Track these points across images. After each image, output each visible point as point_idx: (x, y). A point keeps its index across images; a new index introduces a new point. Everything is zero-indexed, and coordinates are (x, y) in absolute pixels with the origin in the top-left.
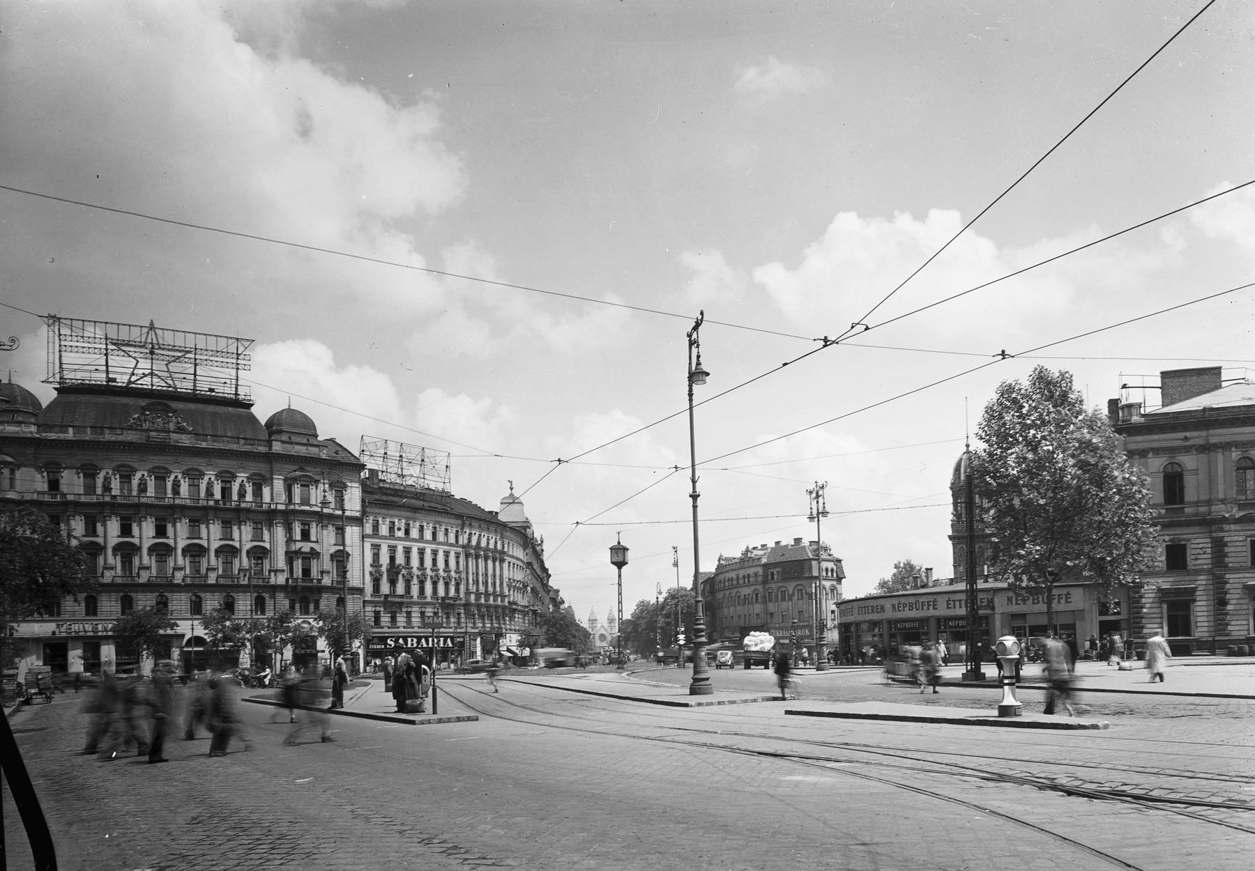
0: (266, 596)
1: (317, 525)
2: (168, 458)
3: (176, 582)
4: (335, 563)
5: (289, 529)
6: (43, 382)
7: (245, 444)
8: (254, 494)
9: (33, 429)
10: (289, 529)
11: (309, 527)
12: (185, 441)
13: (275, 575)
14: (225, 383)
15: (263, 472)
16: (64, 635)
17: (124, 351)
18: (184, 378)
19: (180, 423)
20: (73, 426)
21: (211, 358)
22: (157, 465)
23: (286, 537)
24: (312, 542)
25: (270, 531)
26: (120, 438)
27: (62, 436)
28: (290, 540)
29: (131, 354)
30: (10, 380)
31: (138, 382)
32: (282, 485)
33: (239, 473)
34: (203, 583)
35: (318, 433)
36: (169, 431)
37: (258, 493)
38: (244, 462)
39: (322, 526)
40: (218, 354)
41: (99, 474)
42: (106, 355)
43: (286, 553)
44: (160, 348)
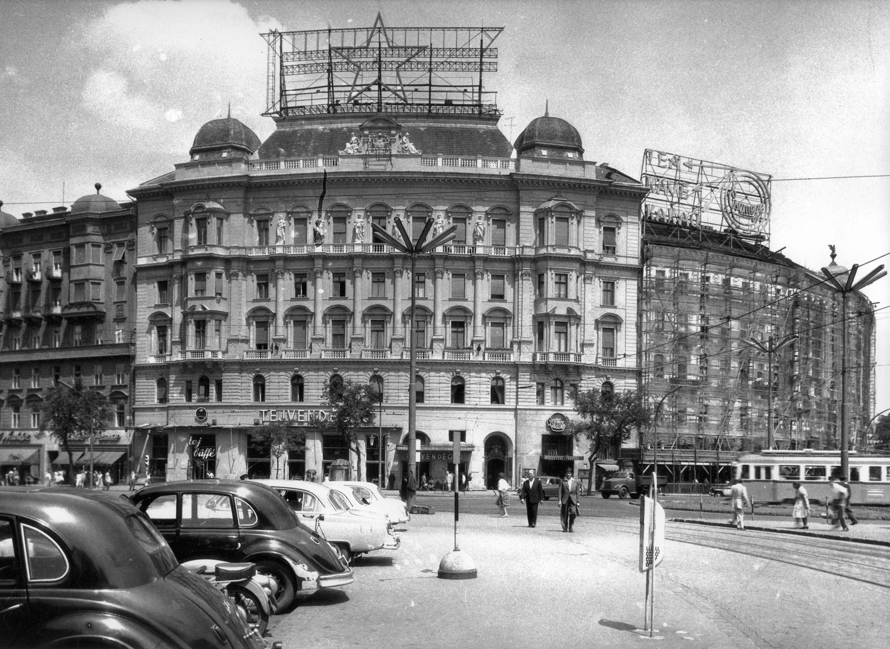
0: (506, 376)
1: (578, 277)
4: (601, 333)
5: (540, 283)
6: (262, 115)
10: (540, 283)
11: (567, 280)
13: (519, 348)
14: (465, 91)
18: (416, 90)
19: (404, 143)
23: (535, 294)
24: (571, 300)
25: (514, 287)
28: (540, 298)
32: (532, 220)
35: (584, 147)
39: (584, 279)
43: (534, 317)
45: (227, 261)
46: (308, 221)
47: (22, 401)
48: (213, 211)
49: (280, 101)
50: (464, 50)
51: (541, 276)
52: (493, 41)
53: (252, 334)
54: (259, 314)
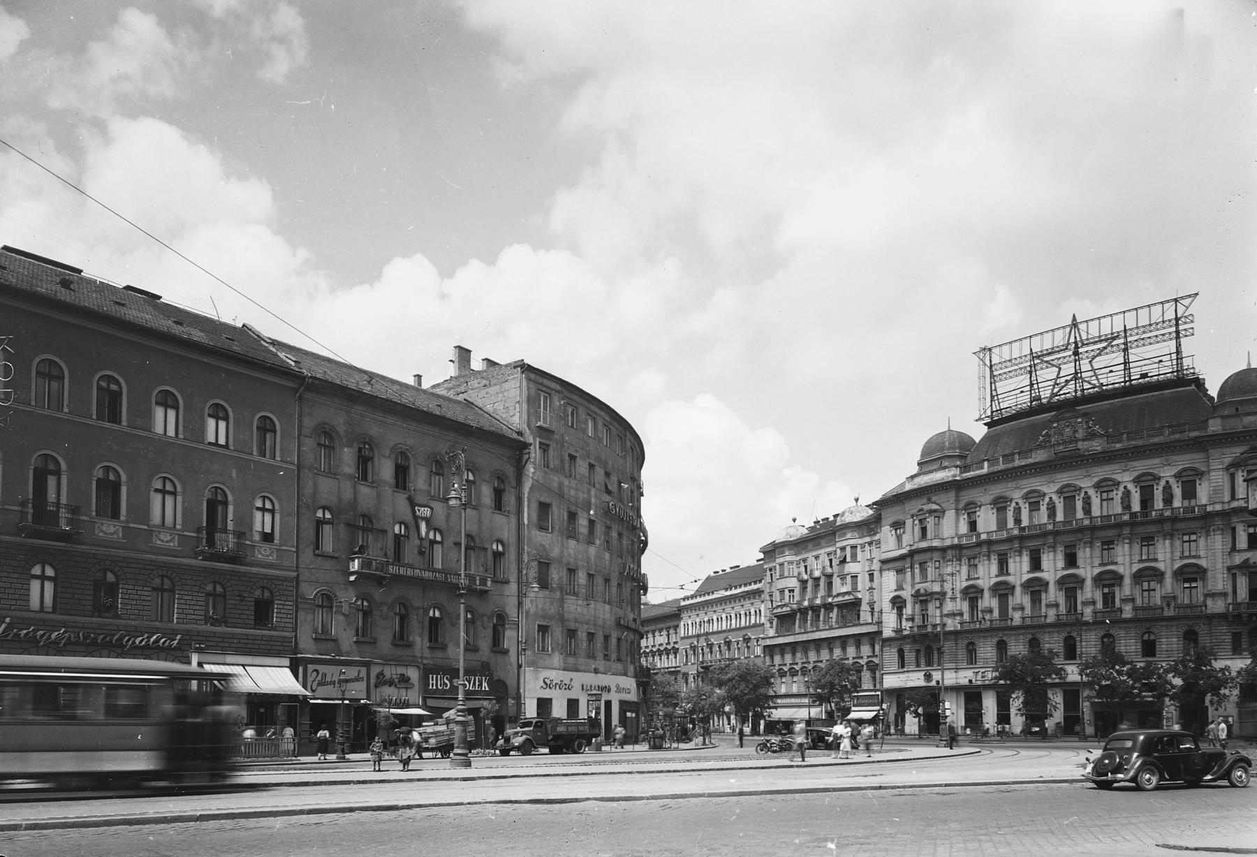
2: (1078, 472)
3: (1084, 619)
7: (1173, 433)
8: (1184, 497)
9: (958, 471)
12: (1096, 448)
14: (1161, 361)
15: (1196, 465)
16: (979, 683)
17: (1046, 362)
18: (1111, 371)
20: (988, 460)
21: (1144, 336)
22: (1101, 477)
26: (1030, 461)
27: (978, 472)
29: (1054, 363)
30: (1249, 364)
31: (1061, 392)
33: (1164, 472)
34: (978, 626)
36: (1077, 440)
37: (1190, 493)
38: (1170, 457)
40: (1152, 328)
41: (1009, 506)
42: (1178, 338)
44: (1083, 345)
45: (943, 550)
48: (931, 512)
49: (991, 405)
50: (1157, 324)
51: (1234, 529)
52: (1187, 308)
53: (965, 607)
54: (971, 590)
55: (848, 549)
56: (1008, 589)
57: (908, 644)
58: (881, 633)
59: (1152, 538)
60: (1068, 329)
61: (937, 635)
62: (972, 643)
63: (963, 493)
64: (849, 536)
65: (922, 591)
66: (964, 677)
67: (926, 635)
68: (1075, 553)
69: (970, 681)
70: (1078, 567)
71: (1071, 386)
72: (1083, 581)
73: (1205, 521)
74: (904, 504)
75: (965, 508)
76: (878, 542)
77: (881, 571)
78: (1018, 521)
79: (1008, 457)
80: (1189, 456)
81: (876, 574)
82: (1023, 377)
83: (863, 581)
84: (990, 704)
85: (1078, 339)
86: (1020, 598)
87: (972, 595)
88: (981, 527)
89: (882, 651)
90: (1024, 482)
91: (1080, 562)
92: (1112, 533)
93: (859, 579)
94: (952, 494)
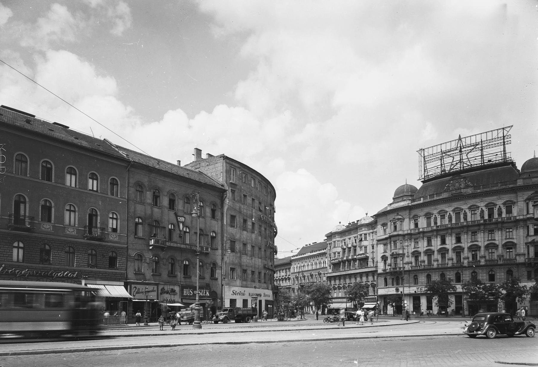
2: (461, 202)
3: (464, 265)
7: (502, 185)
8: (507, 213)
9: (410, 202)
12: (469, 192)
14: (497, 155)
15: (512, 199)
16: (419, 292)
17: (448, 155)
18: (476, 159)
20: (423, 197)
21: (490, 144)
22: (471, 204)
26: (441, 197)
27: (419, 202)
31: (454, 168)
33: (498, 202)
36: (461, 189)
37: (509, 211)
38: (501, 196)
41: (432, 216)
42: (504, 145)
44: (464, 148)
45: (404, 235)
46: (494, 209)
47: (369, 285)
48: (398, 219)
49: (424, 174)
52: (508, 132)
53: (413, 260)
54: (415, 253)
55: (363, 235)
56: (432, 252)
57: (389, 276)
58: (377, 271)
59: (493, 231)
60: (457, 141)
61: (401, 272)
62: (416, 276)
63: (412, 211)
64: (363, 229)
65: (395, 253)
66: (413, 290)
67: (396, 272)
68: (460, 237)
69: (415, 292)
70: (461, 243)
71: (459, 165)
72: (464, 249)
73: (516, 223)
74: (387, 216)
75: (413, 217)
76: (376, 232)
77: (377, 244)
78: (436, 223)
79: (431, 196)
80: (509, 195)
81: (375, 246)
82: (438, 161)
83: (370, 249)
84: (424, 302)
85: (461, 145)
86: (436, 256)
87: (416, 255)
88: (420, 226)
89: (377, 279)
90: (438, 206)
91: (462, 241)
92: (476, 228)
93: (368, 248)
94: (408, 212)
